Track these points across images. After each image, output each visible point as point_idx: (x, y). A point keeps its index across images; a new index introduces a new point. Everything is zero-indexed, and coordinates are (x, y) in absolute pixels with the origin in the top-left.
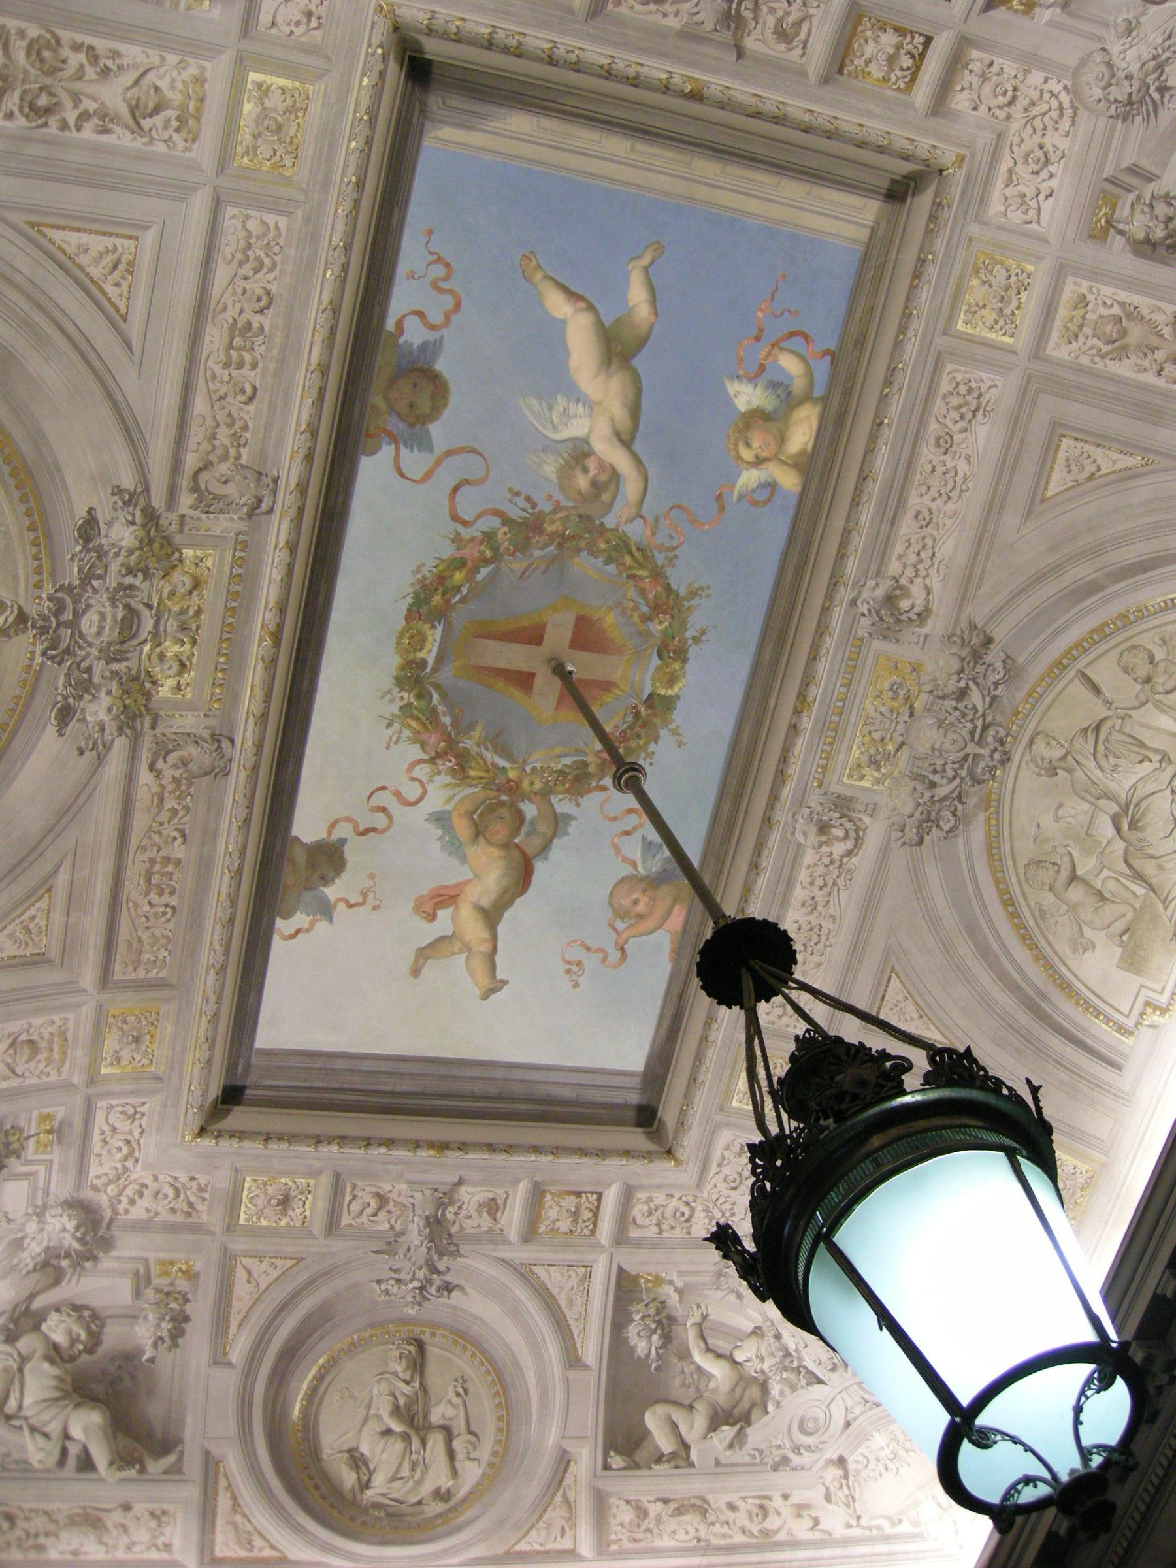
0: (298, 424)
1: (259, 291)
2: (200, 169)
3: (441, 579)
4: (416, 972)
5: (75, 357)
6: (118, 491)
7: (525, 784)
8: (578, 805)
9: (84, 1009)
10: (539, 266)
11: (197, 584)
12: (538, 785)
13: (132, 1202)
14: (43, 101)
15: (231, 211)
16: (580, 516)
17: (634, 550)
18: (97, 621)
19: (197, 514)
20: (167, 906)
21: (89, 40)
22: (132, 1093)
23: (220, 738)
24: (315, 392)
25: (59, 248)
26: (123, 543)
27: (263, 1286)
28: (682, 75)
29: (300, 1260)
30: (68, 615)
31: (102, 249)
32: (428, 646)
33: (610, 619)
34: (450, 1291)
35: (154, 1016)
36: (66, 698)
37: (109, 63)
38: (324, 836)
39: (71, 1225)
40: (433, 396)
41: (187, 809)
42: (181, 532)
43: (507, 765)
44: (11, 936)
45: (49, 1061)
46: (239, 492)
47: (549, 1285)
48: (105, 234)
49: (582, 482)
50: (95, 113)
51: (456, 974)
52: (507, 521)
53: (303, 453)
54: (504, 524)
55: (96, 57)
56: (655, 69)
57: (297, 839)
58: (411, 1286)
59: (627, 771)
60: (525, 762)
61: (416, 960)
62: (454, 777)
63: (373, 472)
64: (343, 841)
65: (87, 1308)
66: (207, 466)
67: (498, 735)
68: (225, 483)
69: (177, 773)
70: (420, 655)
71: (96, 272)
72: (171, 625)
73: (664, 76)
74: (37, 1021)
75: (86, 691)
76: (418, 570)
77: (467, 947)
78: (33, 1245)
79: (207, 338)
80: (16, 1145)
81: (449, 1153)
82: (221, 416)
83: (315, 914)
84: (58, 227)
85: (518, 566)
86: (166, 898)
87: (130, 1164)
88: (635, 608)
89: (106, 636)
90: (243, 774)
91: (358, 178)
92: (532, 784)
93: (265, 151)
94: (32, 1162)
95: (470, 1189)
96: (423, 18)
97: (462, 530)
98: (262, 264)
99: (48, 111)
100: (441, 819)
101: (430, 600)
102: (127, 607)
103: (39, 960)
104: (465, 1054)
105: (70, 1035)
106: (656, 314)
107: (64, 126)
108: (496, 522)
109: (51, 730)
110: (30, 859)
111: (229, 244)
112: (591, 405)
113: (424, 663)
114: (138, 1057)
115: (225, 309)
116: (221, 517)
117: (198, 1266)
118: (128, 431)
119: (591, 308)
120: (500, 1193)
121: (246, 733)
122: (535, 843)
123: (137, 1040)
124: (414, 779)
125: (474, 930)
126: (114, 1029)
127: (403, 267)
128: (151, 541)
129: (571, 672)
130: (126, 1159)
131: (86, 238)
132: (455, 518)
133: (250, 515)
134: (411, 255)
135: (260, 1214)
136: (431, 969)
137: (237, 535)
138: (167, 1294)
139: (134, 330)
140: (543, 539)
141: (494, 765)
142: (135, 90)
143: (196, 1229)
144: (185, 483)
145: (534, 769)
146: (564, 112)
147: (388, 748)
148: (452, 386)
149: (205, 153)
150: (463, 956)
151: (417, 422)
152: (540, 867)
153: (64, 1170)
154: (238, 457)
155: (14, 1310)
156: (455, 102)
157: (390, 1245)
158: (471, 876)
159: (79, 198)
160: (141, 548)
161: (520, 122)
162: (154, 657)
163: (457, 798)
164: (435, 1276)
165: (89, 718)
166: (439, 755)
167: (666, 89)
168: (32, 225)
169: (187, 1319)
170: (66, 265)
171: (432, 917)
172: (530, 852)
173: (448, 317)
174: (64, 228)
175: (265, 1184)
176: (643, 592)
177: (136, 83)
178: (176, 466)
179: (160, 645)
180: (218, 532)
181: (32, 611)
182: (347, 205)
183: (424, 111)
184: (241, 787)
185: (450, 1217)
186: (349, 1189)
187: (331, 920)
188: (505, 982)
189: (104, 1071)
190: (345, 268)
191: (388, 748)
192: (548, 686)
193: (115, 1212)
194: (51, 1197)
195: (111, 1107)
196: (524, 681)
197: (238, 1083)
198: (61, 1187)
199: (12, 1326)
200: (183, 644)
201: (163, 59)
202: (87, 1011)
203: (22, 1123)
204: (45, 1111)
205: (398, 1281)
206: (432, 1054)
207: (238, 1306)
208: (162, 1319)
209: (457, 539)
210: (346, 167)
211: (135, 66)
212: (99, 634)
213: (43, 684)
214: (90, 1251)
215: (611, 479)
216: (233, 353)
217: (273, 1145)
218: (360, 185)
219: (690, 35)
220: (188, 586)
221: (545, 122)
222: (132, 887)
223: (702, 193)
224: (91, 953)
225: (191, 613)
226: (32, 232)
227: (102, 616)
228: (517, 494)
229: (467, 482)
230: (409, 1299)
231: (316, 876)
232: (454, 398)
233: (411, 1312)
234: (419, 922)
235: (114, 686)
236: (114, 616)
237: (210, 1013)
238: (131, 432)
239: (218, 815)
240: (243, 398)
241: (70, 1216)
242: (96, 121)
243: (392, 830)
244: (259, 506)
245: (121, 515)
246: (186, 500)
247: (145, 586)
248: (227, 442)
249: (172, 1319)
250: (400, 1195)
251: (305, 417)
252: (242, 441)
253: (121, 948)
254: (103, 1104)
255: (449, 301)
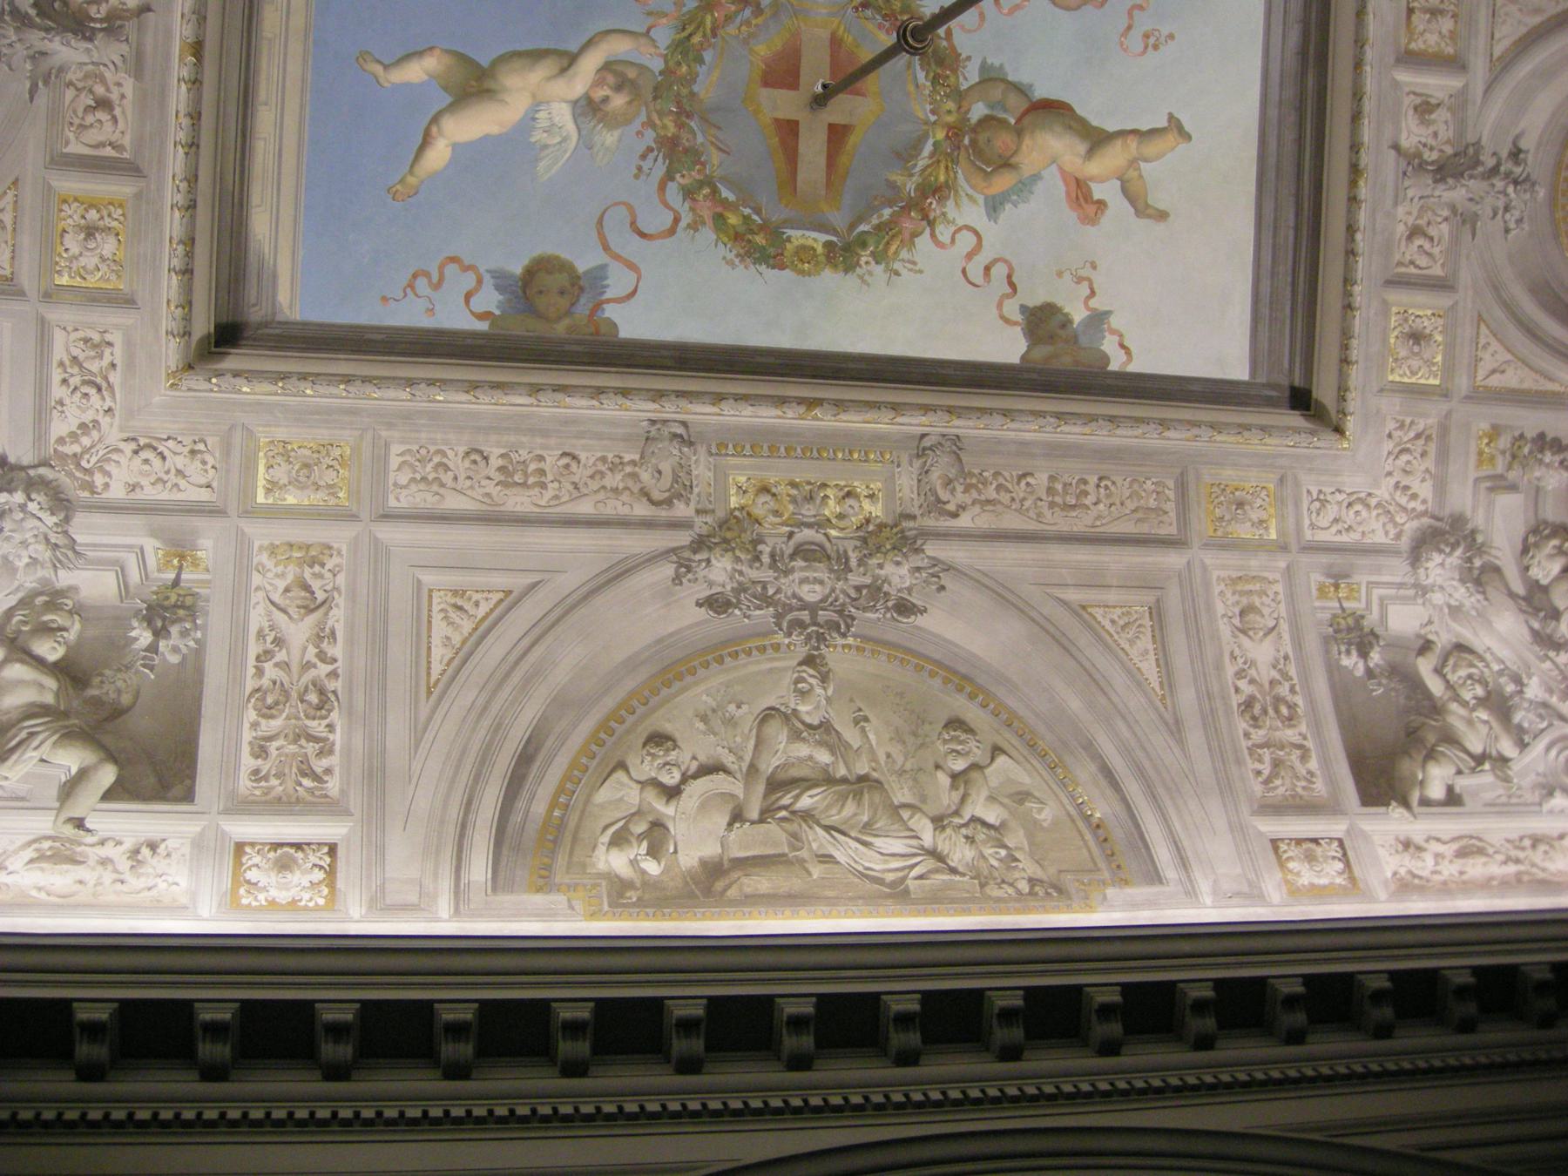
0: (592, 408)
1: (467, 463)
2: (202, 834)
3: (737, 237)
4: (1162, 216)
5: (549, 638)
6: (677, 580)
7: (950, 119)
8: (969, 58)
9: (1208, 561)
10: (402, 181)
11: (765, 490)
12: (951, 105)
13: (1414, 497)
14: (313, 698)
15: (392, 502)
16: (655, 98)
17: (685, 34)
18: (809, 584)
19: (693, 497)
20: (1098, 486)
21: (251, 661)
22: (1297, 505)
23: (921, 449)
24: (559, 396)
25: (448, 664)
26: (729, 568)
27: (1509, 357)
28: (179, 69)
29: (1480, 318)
30: (805, 616)
31: (444, 624)
32: (810, 242)
33: (762, 50)
34: (1520, 151)
35: (1215, 489)
36: (888, 609)
37: (269, 639)
38: (1019, 329)
39: (1437, 558)
40: (549, 272)
41: (997, 474)
42: (713, 511)
43: (931, 141)
44: (1132, 642)
45: (1264, 593)
46: (668, 458)
47: (1516, 37)
48: (430, 622)
49: (619, 101)
50: (317, 647)
51: (1164, 173)
52: (669, 176)
53: (620, 400)
54: (672, 179)
55: (266, 652)
56: (178, 98)
57: (1023, 358)
58: (1513, 195)
59: (907, 42)
60: (927, 123)
61: (1149, 216)
62: (948, 198)
63: (635, 322)
64: (1024, 309)
65: (1525, 540)
66: (645, 493)
67: (898, 155)
68: (660, 472)
69: (960, 489)
70: (820, 250)
71: (467, 626)
72: (808, 511)
73: (184, 87)
74: (1220, 609)
75: (879, 589)
76: (730, 263)
77: (1133, 163)
78: (1457, 595)
79: (518, 508)
80: (1350, 621)
81: (1362, 165)
82: (594, 485)
83: (1102, 331)
84: (429, 668)
85: (715, 157)
86: (1090, 488)
87: (1373, 502)
88: (748, 23)
89: (824, 576)
90: (956, 422)
91: (342, 382)
92: (949, 112)
93: (330, 478)
94: (1369, 603)
95: (1404, 136)
96: (174, 343)
97: (683, 224)
98: (440, 464)
99: (322, 692)
100: (994, 207)
101: (761, 246)
102: (792, 557)
103: (1157, 613)
104: (1253, 152)
105: (1235, 574)
106: (431, 49)
107: (334, 674)
108: (672, 188)
109: (920, 620)
110: (1052, 630)
111: (422, 499)
112: (537, 105)
113: (828, 244)
114: (1259, 502)
115: (488, 495)
116: (695, 473)
117: (1485, 426)
118: (618, 576)
119: (435, 119)
120: (1409, 101)
121: (914, 424)
122: (1014, 100)
123: (1240, 505)
124: (953, 240)
125: (1114, 157)
126: (1229, 529)
127: (426, 322)
128: (725, 541)
129: (825, 86)
130: (1368, 506)
131: (436, 641)
132: (672, 231)
133: (691, 444)
134: (410, 315)
135: (1429, 363)
136: (1158, 200)
137: (711, 454)
138: (1514, 457)
139: (519, 582)
140: (685, 136)
141: (932, 155)
142: (290, 611)
143: (1444, 430)
144: (664, 513)
145: (933, 112)
146: (242, 184)
147: (921, 272)
148: (537, 253)
149: (340, 536)
150: (1142, 164)
151: (579, 285)
152: (1040, 93)
153: (1378, 570)
154: (633, 463)
155: (1524, 612)
156: (251, 293)
157: (1466, 220)
158: (1054, 168)
159: (400, 652)
160: (733, 550)
161: (260, 225)
162: (842, 524)
163: (970, 192)
164: (1502, 169)
165: (907, 584)
166: (925, 217)
167: (196, 82)
168: (429, 693)
169: (1542, 436)
170: (463, 656)
171: (1101, 204)
172: (1025, 105)
173: (466, 268)
174: (429, 663)
175: (1396, 360)
176: (729, 19)
177: (284, 611)
178: (648, 524)
179: (829, 520)
180: (711, 474)
181: (802, 651)
182: (369, 389)
183: (266, 325)
184: (971, 423)
185: (1434, 156)
186: (1402, 270)
187: (1108, 313)
188: (1171, 117)
189: (1273, 536)
190: (431, 382)
191: (921, 272)
192: (840, 109)
193: (1424, 513)
194: (1406, 580)
195: (1313, 527)
196: (837, 134)
197: (1287, 394)
198: (1397, 571)
199: (1542, 614)
200: (826, 497)
201: (258, 588)
202: (1209, 558)
203: (1327, 616)
204: (1314, 592)
205: (1507, 209)
206: (1252, 188)
207: (1530, 382)
208: (1541, 462)
209: (694, 226)
210: (332, 396)
211: (269, 614)
212: (821, 582)
213: (874, 633)
214: (1465, 538)
215: (615, 73)
216: (531, 480)
217: (1354, 354)
218: (348, 379)
219: (137, 66)
220: (768, 498)
221: (255, 199)
222: (1079, 523)
223: (298, 21)
224: (1150, 559)
225: (794, 492)
226: (436, 692)
227: (803, 581)
228: (640, 169)
229: (633, 223)
230: (1528, 196)
231: (1062, 333)
232: (549, 249)
233: (1542, 193)
234: (1106, 220)
235: (874, 561)
236: (802, 569)
237: (1210, 432)
238: (619, 572)
239: (999, 442)
240: (574, 465)
241: (1428, 560)
242: (324, 645)
243: (1008, 257)
244: (681, 436)
245: (701, 574)
246: (681, 510)
247: (771, 541)
248: (619, 477)
249: (1541, 451)
250: (1409, 213)
251: (584, 402)
252: (617, 460)
253: (1144, 528)
254: (1308, 535)
255: (451, 269)
